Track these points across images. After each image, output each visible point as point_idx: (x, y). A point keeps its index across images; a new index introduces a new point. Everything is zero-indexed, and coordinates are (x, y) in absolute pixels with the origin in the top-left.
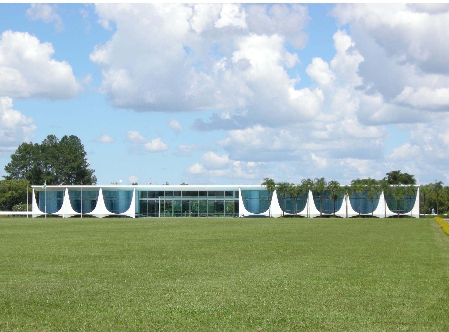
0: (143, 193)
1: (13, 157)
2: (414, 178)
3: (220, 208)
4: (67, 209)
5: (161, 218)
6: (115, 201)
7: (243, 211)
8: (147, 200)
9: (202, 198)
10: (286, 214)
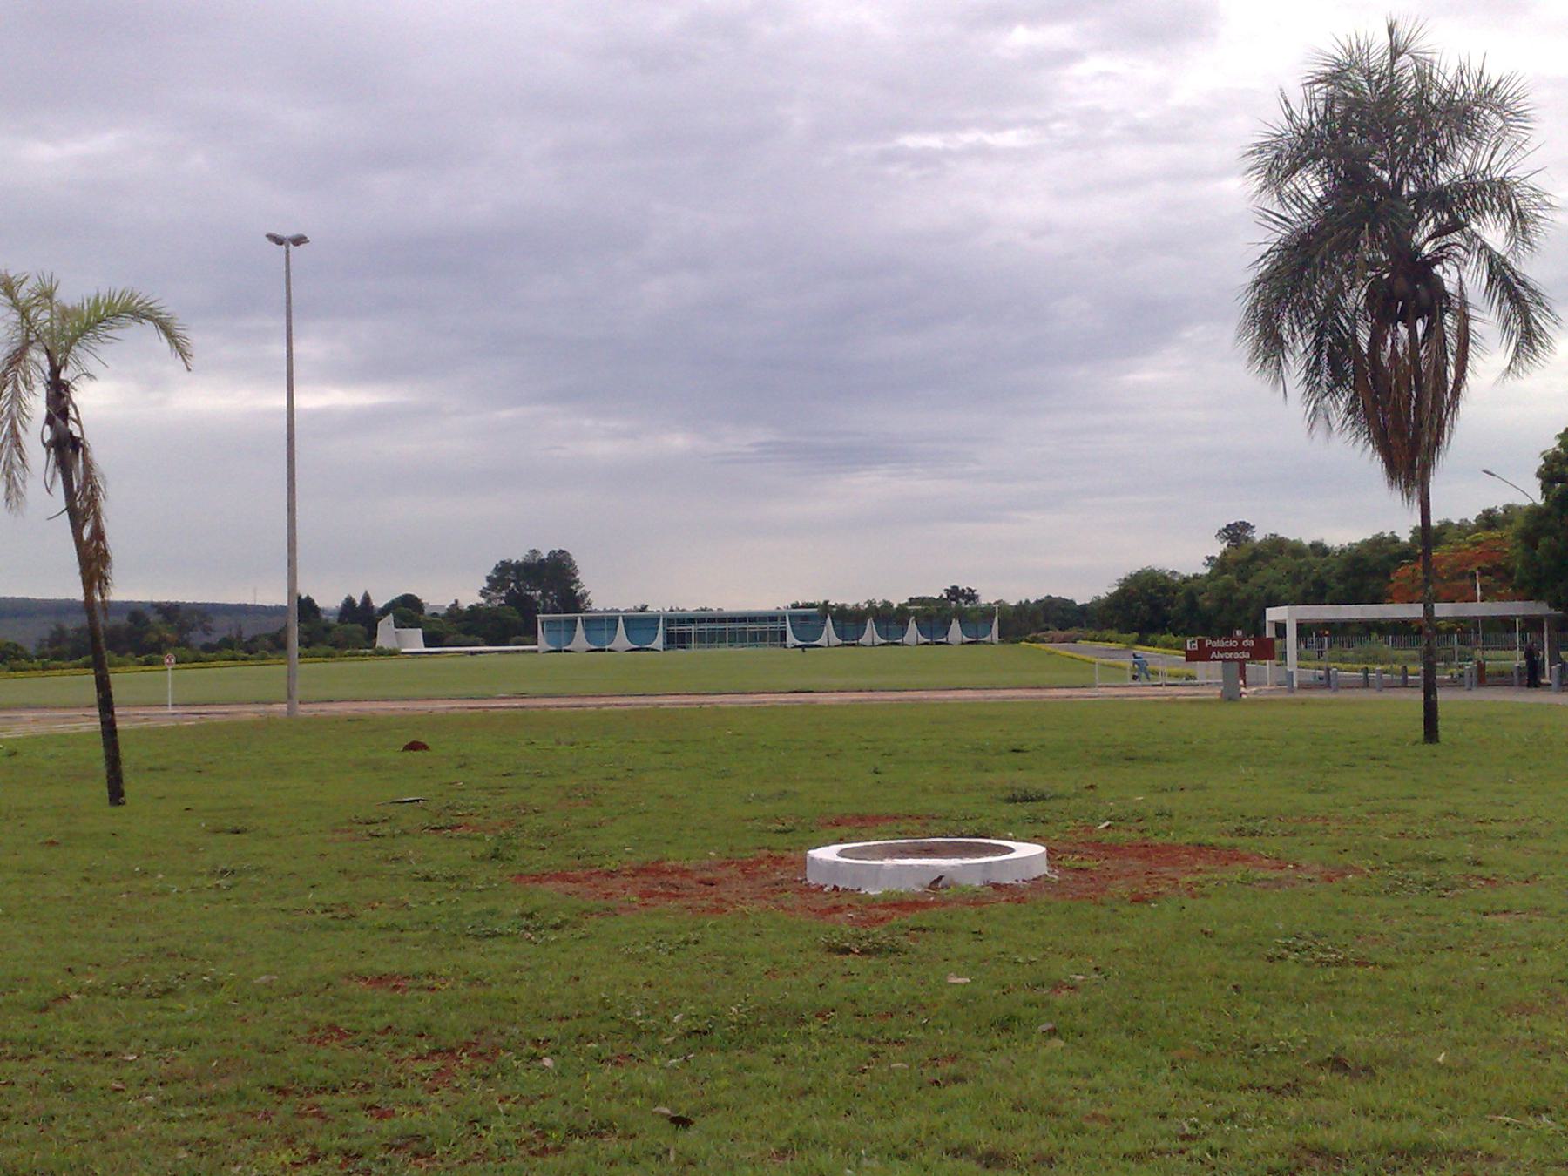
0: (669, 621)
1: (489, 579)
2: (1454, 50)
3: (758, 638)
4: (580, 640)
5: (694, 651)
6: (603, 624)
7: (791, 639)
8: (675, 629)
9: (742, 625)
10: (923, 639)
